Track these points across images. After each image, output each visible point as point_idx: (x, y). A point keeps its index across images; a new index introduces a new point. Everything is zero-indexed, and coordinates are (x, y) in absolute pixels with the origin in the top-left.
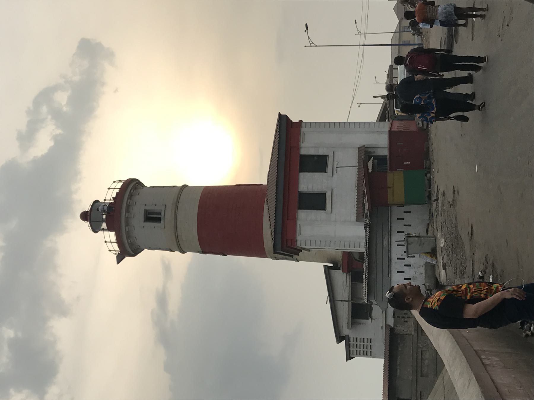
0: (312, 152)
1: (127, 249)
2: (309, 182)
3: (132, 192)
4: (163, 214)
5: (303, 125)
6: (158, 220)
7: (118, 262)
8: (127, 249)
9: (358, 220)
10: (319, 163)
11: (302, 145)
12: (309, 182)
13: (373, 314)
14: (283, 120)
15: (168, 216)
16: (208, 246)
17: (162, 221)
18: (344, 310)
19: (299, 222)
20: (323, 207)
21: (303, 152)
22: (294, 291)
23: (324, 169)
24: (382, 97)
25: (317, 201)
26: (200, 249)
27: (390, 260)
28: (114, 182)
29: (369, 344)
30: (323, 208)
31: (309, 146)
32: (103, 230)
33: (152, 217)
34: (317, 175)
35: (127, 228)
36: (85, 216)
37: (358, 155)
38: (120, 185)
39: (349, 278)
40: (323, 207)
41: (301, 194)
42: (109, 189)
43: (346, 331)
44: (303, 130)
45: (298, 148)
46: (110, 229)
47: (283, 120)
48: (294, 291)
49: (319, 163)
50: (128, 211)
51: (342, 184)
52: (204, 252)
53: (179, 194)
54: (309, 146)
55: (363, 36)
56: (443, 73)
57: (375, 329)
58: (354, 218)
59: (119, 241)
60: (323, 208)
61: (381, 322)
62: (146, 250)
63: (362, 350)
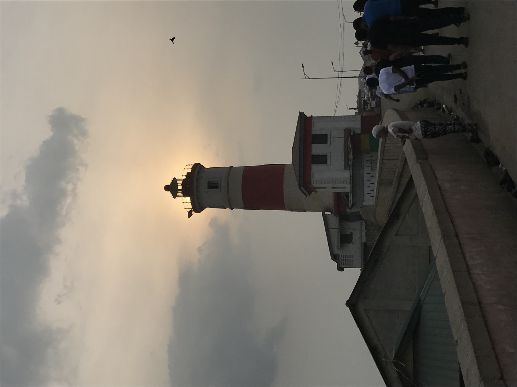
0: (318, 133)
1: (197, 207)
2: (317, 149)
4: (219, 183)
5: (313, 118)
6: (217, 187)
7: (189, 217)
8: (197, 207)
9: (345, 168)
10: (322, 139)
12: (317, 149)
13: (353, 240)
14: (302, 115)
17: (219, 188)
20: (325, 162)
21: (314, 133)
22: (302, 231)
23: (325, 142)
24: (355, 109)
25: (322, 160)
26: (243, 205)
27: (363, 181)
29: (351, 258)
30: (326, 163)
31: (316, 130)
32: (179, 196)
33: (213, 186)
34: (321, 145)
36: (167, 188)
40: (325, 162)
41: (313, 156)
43: (336, 251)
45: (311, 131)
46: (185, 195)
47: (302, 115)
48: (302, 231)
49: (322, 139)
51: (335, 149)
52: (246, 208)
54: (316, 130)
55: (340, 73)
57: (354, 249)
58: (343, 168)
59: (192, 202)
60: (326, 163)
61: (359, 245)
62: (207, 209)
63: (347, 262)
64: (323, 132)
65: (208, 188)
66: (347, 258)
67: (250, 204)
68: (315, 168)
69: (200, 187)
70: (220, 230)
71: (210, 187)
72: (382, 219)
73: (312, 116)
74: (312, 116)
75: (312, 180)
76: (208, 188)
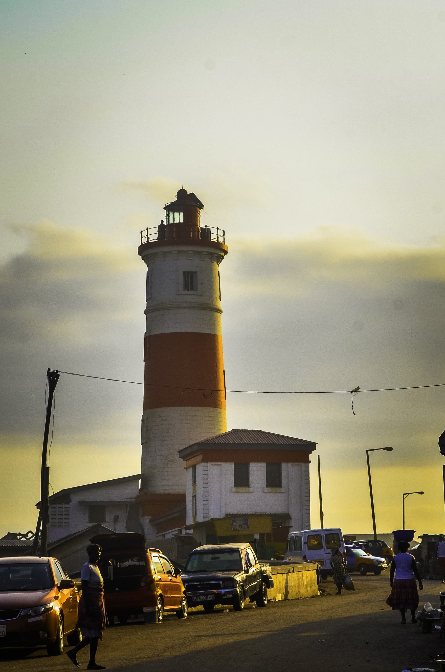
2: (257, 471)
3: (204, 253)
11: (290, 464)
12: (257, 471)
15: (190, 297)
16: (151, 342)
18: (352, 591)
19: (223, 464)
21: (284, 466)
25: (242, 480)
28: (224, 231)
31: (288, 470)
35: (192, 252)
37: (231, 513)
38: (221, 240)
39: (133, 500)
42: (218, 229)
44: (303, 465)
45: (287, 461)
47: (312, 446)
49: (274, 481)
50: (195, 252)
51: (258, 499)
53: (194, 308)
54: (288, 470)
56: (91, 525)
64: (284, 481)
65: (184, 273)
66: (64, 517)
67: (155, 346)
68: (228, 469)
69: (183, 247)
70: (216, 420)
71: (186, 274)
72: (197, 556)
73: (310, 462)
74: (310, 462)
75: (210, 464)
76: (184, 273)
